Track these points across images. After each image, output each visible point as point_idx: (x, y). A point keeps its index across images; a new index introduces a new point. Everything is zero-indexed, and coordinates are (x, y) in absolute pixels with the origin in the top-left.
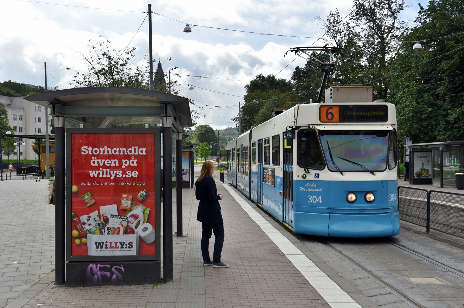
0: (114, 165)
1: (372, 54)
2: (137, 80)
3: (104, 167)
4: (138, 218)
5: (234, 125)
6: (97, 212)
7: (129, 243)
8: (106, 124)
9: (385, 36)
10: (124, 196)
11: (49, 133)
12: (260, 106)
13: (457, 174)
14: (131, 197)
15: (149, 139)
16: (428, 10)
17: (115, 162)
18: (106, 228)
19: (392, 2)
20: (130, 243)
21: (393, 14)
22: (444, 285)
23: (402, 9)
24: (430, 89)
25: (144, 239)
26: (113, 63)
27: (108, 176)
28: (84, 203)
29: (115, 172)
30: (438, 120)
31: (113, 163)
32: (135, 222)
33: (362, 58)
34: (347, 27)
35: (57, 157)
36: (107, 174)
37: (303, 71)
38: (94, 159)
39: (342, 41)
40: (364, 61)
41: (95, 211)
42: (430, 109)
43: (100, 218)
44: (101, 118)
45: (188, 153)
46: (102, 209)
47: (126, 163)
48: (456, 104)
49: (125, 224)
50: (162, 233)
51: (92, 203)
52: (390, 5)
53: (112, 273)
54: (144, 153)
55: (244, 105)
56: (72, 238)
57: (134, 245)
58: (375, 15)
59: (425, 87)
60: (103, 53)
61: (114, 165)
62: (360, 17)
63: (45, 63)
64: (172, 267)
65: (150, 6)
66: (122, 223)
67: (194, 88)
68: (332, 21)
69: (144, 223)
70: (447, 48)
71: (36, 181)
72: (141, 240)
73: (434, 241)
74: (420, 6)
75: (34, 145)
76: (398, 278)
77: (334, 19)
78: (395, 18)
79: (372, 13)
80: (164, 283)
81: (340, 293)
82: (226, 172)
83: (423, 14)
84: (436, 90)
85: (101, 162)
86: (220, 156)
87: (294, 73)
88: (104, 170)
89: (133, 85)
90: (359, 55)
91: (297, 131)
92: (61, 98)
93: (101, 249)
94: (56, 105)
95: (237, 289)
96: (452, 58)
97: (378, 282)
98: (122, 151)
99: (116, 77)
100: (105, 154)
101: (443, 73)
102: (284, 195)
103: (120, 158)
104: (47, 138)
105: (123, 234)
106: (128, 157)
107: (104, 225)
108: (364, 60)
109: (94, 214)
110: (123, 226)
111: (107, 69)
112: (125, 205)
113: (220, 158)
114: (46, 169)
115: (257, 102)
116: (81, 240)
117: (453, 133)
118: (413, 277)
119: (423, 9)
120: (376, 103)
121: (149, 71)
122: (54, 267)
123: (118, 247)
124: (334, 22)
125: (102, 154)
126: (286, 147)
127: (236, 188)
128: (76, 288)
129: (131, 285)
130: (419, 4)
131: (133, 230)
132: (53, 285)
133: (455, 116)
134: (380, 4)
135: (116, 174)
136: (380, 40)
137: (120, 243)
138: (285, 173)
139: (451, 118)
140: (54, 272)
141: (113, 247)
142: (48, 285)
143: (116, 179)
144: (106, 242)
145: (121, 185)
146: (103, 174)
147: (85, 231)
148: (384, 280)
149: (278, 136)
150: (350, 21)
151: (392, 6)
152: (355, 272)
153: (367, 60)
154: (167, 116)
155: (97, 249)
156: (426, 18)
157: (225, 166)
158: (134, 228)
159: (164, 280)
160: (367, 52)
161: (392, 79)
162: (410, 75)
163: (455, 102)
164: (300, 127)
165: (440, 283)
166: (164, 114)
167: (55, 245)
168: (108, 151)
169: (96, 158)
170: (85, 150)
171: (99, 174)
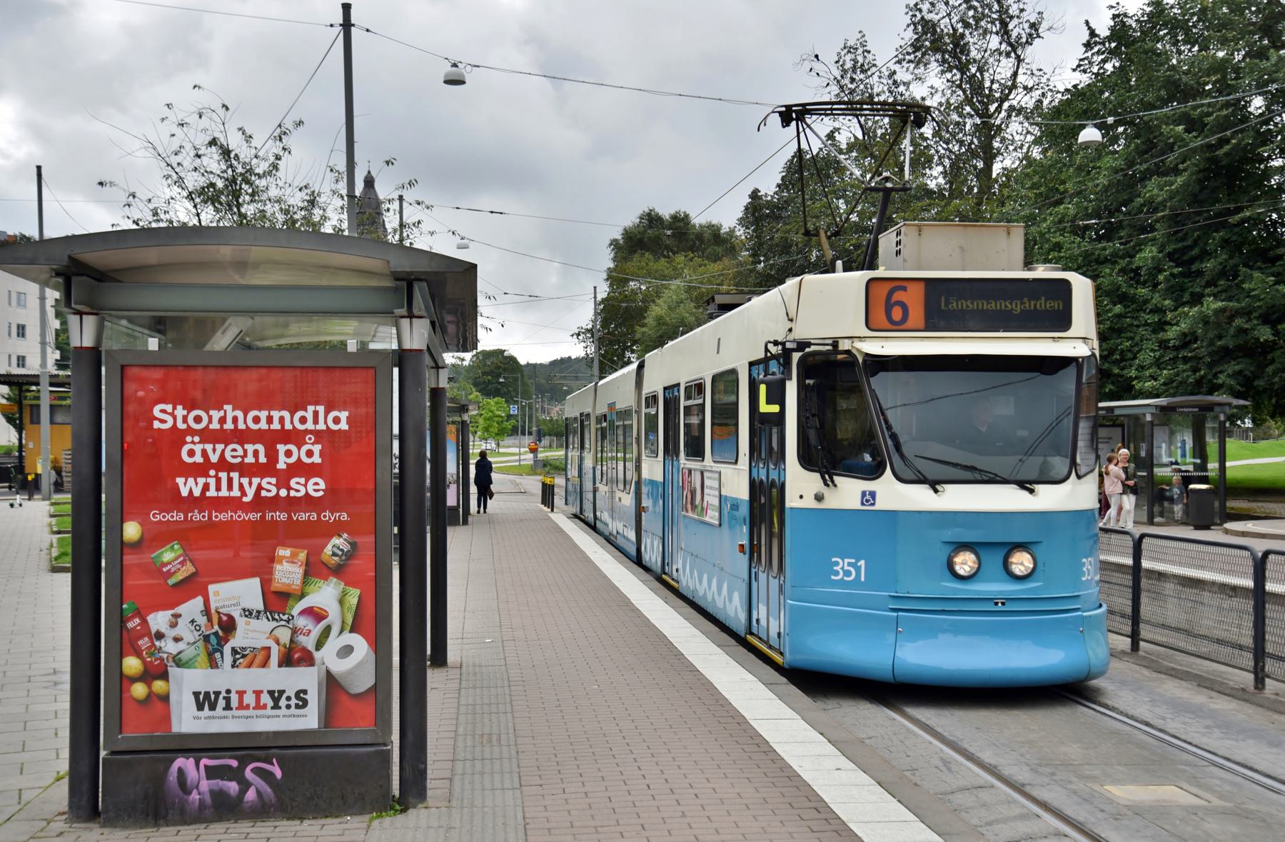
1: (958, 157)
2: (307, 220)
3: (223, 465)
4: (324, 617)
5: (577, 350)
6: (200, 599)
7: (297, 694)
8: (221, 342)
10: (284, 552)
11: (52, 369)
14: (302, 555)
15: (356, 385)
16: (1109, 39)
17: (254, 452)
18: (227, 649)
19: (1011, 18)
20: (301, 694)
21: (1014, 48)
22: (1205, 808)
23: (1039, 36)
24: (1115, 254)
26: (240, 170)
27: (236, 493)
28: (159, 572)
29: (256, 481)
30: (1137, 338)
31: (250, 454)
32: (317, 630)
33: (931, 168)
34: (890, 82)
35: (76, 437)
36: (230, 487)
37: (771, 201)
38: (193, 442)
40: (936, 178)
42: (1118, 309)
43: (210, 620)
44: (207, 324)
46: (216, 593)
47: (288, 454)
48: (1186, 297)
49: (284, 635)
50: (396, 658)
51: (186, 574)
52: (1004, 25)
53: (245, 785)
54: (344, 426)
55: (605, 295)
56: (124, 681)
57: (313, 698)
58: (965, 49)
59: (1104, 249)
60: (210, 139)
62: (924, 54)
63: (39, 168)
64: (425, 763)
65: (347, 8)
66: (276, 632)
67: (471, 244)
68: (849, 65)
70: (1161, 145)
71: (12, 505)
72: (332, 684)
73: (1155, 675)
74: (1089, 28)
75: (4, 402)
77: (855, 61)
79: (956, 45)
82: (559, 481)
83: (1096, 49)
84: (1132, 256)
85: (214, 450)
86: (540, 435)
87: (747, 208)
88: (223, 475)
91: (796, 356)
92: (92, 257)
93: (212, 713)
94: (74, 279)
95: (619, 829)
96: (1176, 171)
98: (276, 420)
99: (249, 210)
100: (225, 427)
102: (753, 551)
103: (271, 439)
104: (45, 382)
105: (280, 666)
106: (295, 437)
107: (222, 641)
108: (935, 173)
109: (192, 608)
110: (278, 642)
112: (284, 580)
114: (39, 471)
115: (643, 288)
116: (149, 686)
118: (1116, 782)
119: (1098, 36)
120: (1042, 272)
122: (64, 766)
124: (854, 69)
125: (218, 427)
126: (764, 408)
127: (593, 527)
129: (302, 819)
130: (1087, 23)
131: (310, 653)
132: (61, 824)
133: (1184, 326)
134: (978, 20)
135: (260, 488)
136: (978, 121)
137: (271, 693)
138: (755, 487)
139: (1172, 333)
140: (66, 780)
141: (248, 707)
142: (44, 823)
143: (260, 502)
144: (228, 691)
145: (273, 521)
146: (218, 489)
147: (162, 659)
148: (1036, 793)
149: (733, 372)
151: (1011, 27)
152: (949, 769)
154: (411, 316)
155: (200, 714)
156: (1104, 61)
158: (311, 647)
159: (399, 802)
162: (1064, 216)
163: (1183, 290)
164: (809, 344)
166: (403, 311)
167: (67, 698)
168: (235, 420)
169: (197, 439)
170: (166, 416)
171: (206, 487)
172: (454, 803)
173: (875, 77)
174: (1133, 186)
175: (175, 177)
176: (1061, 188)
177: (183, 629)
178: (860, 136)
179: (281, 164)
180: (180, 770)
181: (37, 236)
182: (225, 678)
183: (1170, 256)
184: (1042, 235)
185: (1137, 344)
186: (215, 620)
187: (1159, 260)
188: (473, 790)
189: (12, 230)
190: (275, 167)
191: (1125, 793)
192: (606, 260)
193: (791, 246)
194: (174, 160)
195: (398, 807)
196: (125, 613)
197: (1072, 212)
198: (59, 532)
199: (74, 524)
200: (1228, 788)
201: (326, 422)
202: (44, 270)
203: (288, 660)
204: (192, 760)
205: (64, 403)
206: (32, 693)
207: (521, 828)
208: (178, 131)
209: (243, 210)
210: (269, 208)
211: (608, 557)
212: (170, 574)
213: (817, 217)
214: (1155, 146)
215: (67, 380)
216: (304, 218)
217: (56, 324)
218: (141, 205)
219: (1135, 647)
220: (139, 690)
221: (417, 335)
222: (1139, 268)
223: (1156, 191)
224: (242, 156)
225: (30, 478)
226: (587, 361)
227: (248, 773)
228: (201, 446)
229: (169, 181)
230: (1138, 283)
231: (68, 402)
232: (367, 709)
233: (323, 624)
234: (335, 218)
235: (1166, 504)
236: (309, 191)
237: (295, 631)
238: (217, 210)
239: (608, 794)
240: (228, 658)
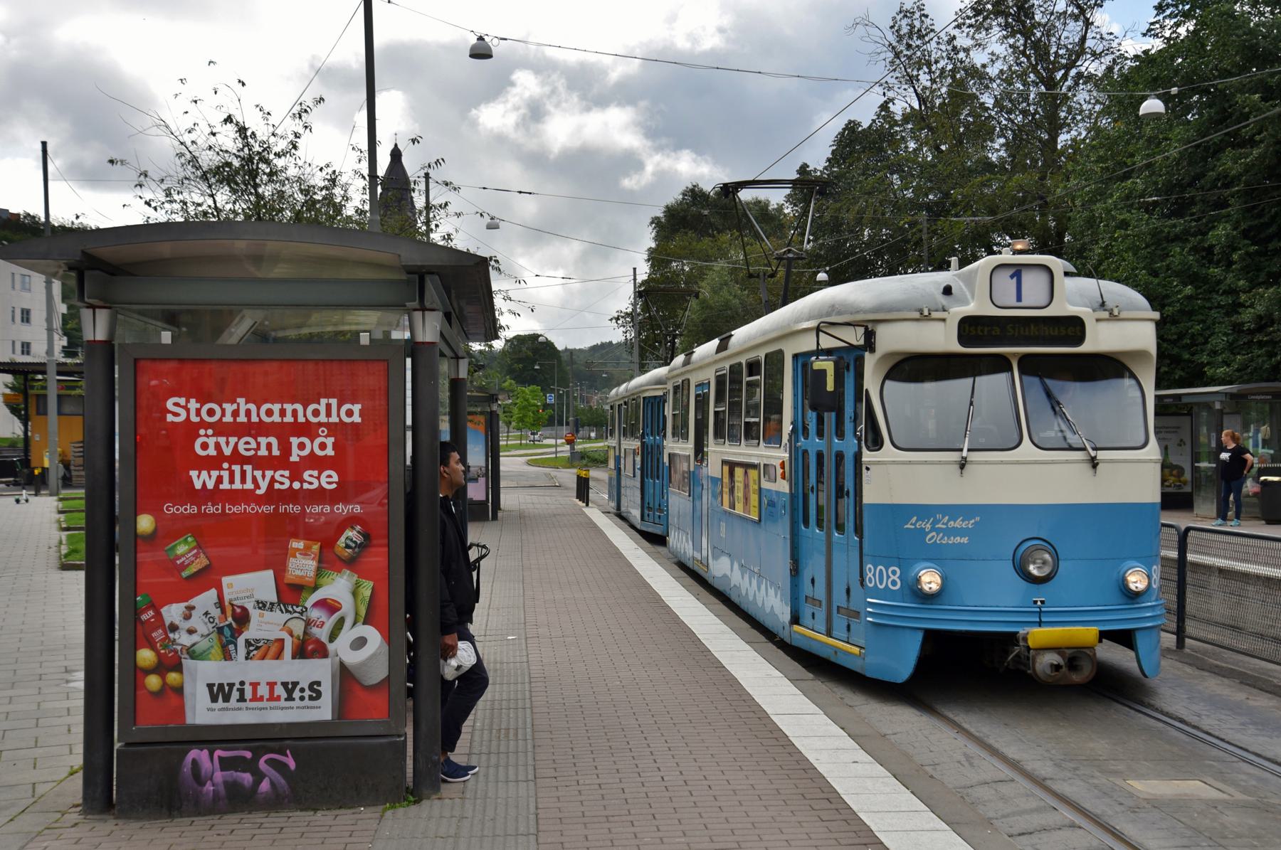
1: (1021, 128)
2: (329, 199)
3: (236, 458)
4: (339, 609)
5: (617, 335)
8: (237, 332)
9: (1059, 75)
10: (297, 544)
11: (59, 356)
17: (267, 445)
18: (241, 641)
20: (314, 687)
24: (1186, 232)
26: (257, 148)
27: (249, 485)
28: (174, 567)
29: (269, 473)
31: (263, 446)
32: (330, 622)
33: (992, 141)
34: (950, 48)
36: (243, 480)
39: (933, 91)
42: (1189, 290)
44: (221, 317)
45: (482, 419)
46: (230, 586)
49: (298, 627)
53: (259, 776)
54: (357, 418)
55: (645, 277)
56: (138, 673)
57: (326, 690)
59: (1174, 226)
60: (225, 116)
62: (985, 19)
63: (44, 144)
66: (289, 624)
67: (501, 224)
68: (905, 30)
69: (355, 624)
71: (18, 501)
72: (345, 675)
73: (1197, 672)
75: (8, 391)
77: (912, 26)
78: (1088, 24)
80: (415, 802)
81: (927, 827)
82: (594, 473)
83: (1168, 12)
84: (1205, 234)
85: (227, 443)
86: (578, 426)
88: (236, 468)
90: (983, 131)
92: (104, 251)
93: (226, 705)
94: (87, 274)
96: (1252, 143)
98: (289, 413)
99: (267, 191)
100: (239, 420)
103: (284, 432)
104: (52, 370)
105: (294, 657)
106: (307, 430)
107: (236, 633)
109: (206, 600)
110: (291, 635)
112: (298, 573)
113: (577, 431)
114: (46, 465)
115: (687, 269)
116: (163, 678)
117: (1252, 360)
118: (1140, 777)
122: (78, 760)
123: (278, 698)
124: (910, 34)
128: (147, 824)
129: (315, 810)
132: (76, 816)
133: (1260, 308)
135: (273, 480)
137: (285, 685)
139: (1246, 316)
140: (80, 774)
141: (261, 699)
142: (59, 815)
143: (273, 495)
144: (242, 683)
146: (232, 481)
147: (175, 651)
148: (1056, 787)
150: (956, 32)
152: (971, 764)
153: (1006, 145)
154: (423, 309)
155: (214, 705)
156: (1177, 25)
157: (591, 455)
158: (324, 639)
160: (1004, 122)
161: (1078, 203)
163: (1259, 270)
165: (1215, 794)
166: (415, 304)
168: (248, 413)
170: (179, 409)
171: (220, 480)
173: (933, 44)
174: (1204, 159)
176: (1129, 161)
177: (197, 621)
178: (917, 107)
179: (301, 143)
181: (43, 219)
182: (240, 670)
183: (1245, 234)
184: (1108, 211)
185: (1209, 328)
186: (229, 612)
188: (487, 782)
189: (15, 208)
190: (295, 147)
191: (1142, 787)
193: (841, 225)
194: (187, 138)
195: (411, 798)
196: (139, 605)
197: (1140, 187)
198: (67, 529)
199: (89, 519)
201: (339, 415)
203: (302, 651)
205: (73, 393)
206: (43, 706)
207: (532, 817)
209: (260, 190)
210: (286, 188)
211: (641, 552)
212: (183, 567)
213: (869, 193)
214: (1231, 115)
215: (76, 369)
216: (325, 198)
217: (63, 308)
218: (153, 185)
219: (1180, 643)
221: (429, 329)
222: (1212, 247)
224: (260, 137)
225: (36, 472)
226: (627, 345)
227: (262, 765)
229: (183, 160)
230: (1210, 262)
231: (78, 391)
234: (356, 199)
236: (330, 170)
237: (308, 623)
238: (234, 191)
239: (622, 785)
240: (242, 650)
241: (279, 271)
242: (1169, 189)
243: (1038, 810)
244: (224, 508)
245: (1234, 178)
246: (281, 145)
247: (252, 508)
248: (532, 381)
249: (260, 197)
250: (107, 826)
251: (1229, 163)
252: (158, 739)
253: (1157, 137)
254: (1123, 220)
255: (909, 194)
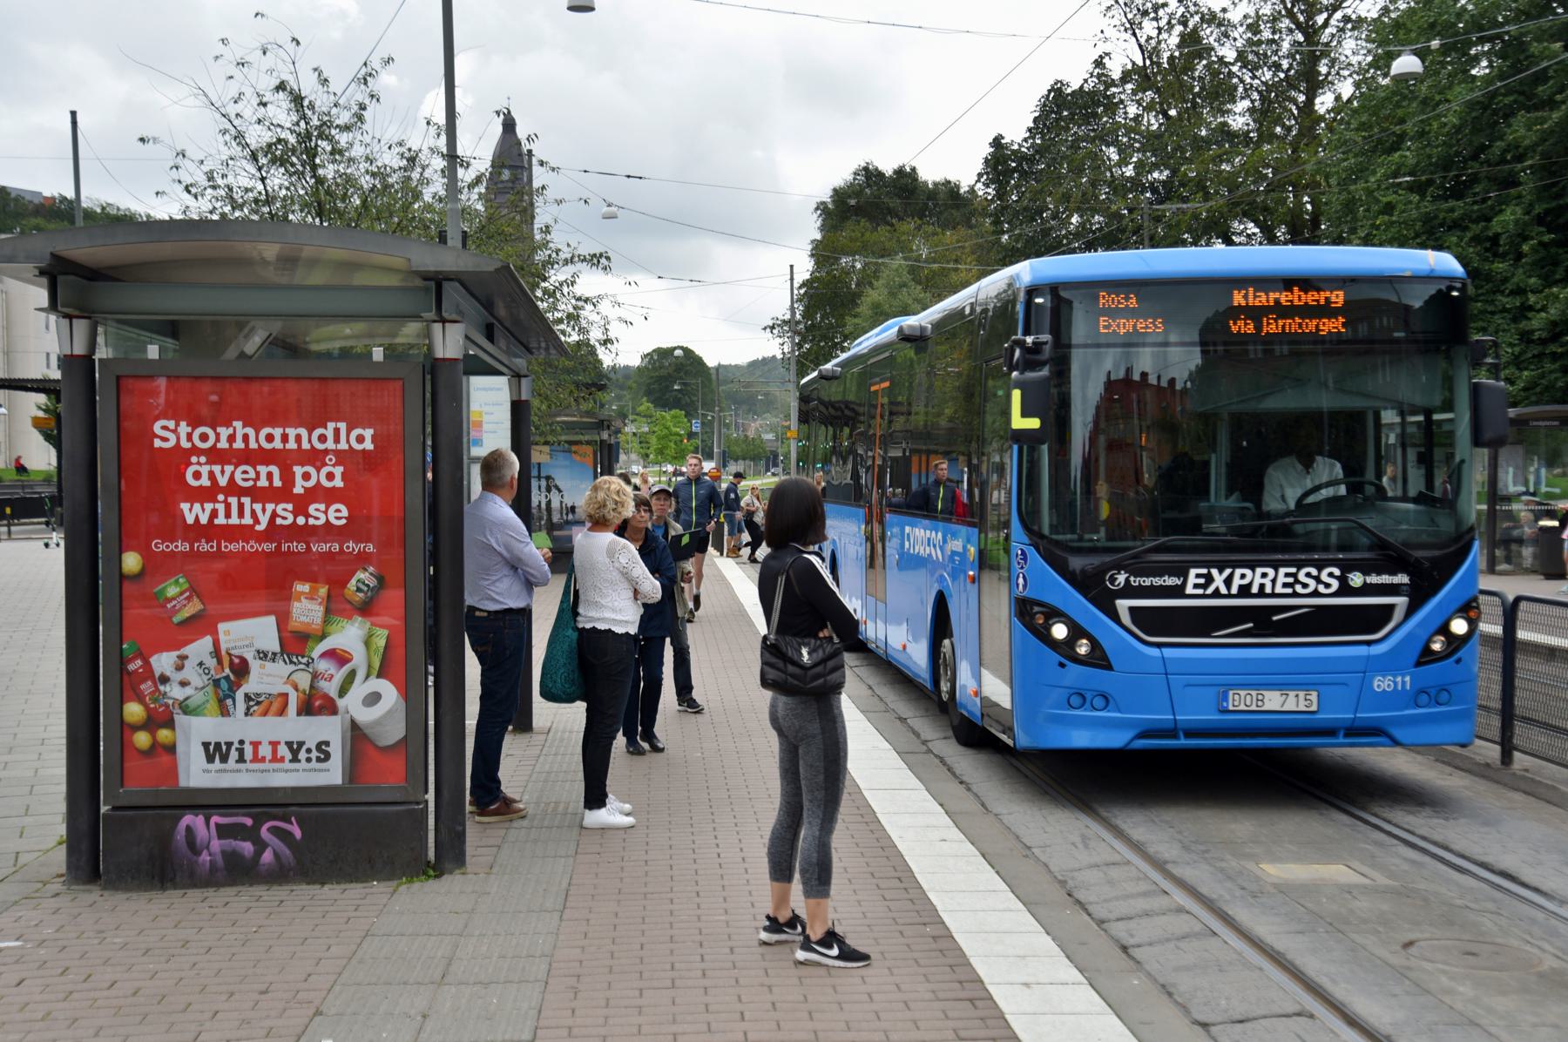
0: (266, 484)
3: (233, 489)
6: (208, 639)
7: (319, 746)
9: (1320, 19)
10: (302, 587)
12: (867, 279)
13: (1542, 523)
14: (323, 591)
17: (268, 475)
18: (240, 695)
20: (322, 747)
22: (1365, 887)
25: (367, 731)
26: (315, 122)
27: (248, 520)
29: (270, 507)
32: (340, 675)
37: (1018, 151)
38: (199, 463)
41: (202, 635)
43: (220, 662)
46: (227, 633)
49: (304, 680)
53: (261, 846)
54: (368, 445)
55: (807, 276)
56: (124, 729)
57: (336, 750)
59: (1452, 210)
60: (277, 82)
61: (266, 484)
63: (73, 114)
66: (294, 677)
67: (620, 213)
69: (367, 677)
71: (47, 545)
72: (357, 734)
75: (41, 414)
76: (1224, 865)
80: (436, 877)
84: (1489, 220)
85: (223, 472)
87: (987, 161)
88: (233, 501)
89: (389, 206)
90: (1221, 91)
93: (223, 766)
94: (60, 279)
97: (1155, 876)
98: (292, 439)
99: (328, 171)
100: (235, 446)
101: (1520, 158)
103: (283, 460)
105: (299, 714)
106: (315, 458)
107: (234, 686)
109: (200, 648)
110: (296, 688)
111: (292, 139)
112: (303, 619)
113: (725, 466)
115: (858, 266)
117: (1542, 376)
121: (445, 150)
123: (282, 759)
125: (227, 446)
128: (134, 895)
129: (323, 884)
131: (331, 701)
133: (1554, 312)
135: (274, 515)
136: (1300, 38)
137: (289, 744)
139: (1537, 322)
144: (242, 742)
145: (289, 553)
146: (228, 516)
147: (167, 706)
152: (1086, 846)
153: (1252, 110)
155: (210, 766)
158: (333, 694)
161: (1333, 181)
162: (1400, 166)
163: (1556, 263)
165: (1355, 879)
166: (432, 315)
168: (246, 438)
169: (203, 459)
170: (168, 434)
171: (214, 514)
172: (495, 870)
175: (233, 132)
180: (189, 829)
182: (238, 727)
183: (1540, 220)
184: (1369, 192)
187: (1525, 224)
190: (360, 118)
191: (1274, 871)
192: (812, 229)
194: (232, 110)
200: (1406, 867)
202: (30, 268)
204: (201, 818)
206: (41, 772)
208: (235, 71)
220: (142, 739)
222: (1497, 236)
223: (1522, 131)
224: (318, 104)
228: (207, 468)
229: (227, 137)
230: (1496, 255)
232: (398, 764)
233: (347, 668)
235: (1514, 547)
237: (315, 676)
241: (318, 278)
242: (1446, 165)
243: (1145, 894)
244: (219, 545)
245: (1527, 148)
246: (344, 118)
247: (253, 546)
248: (676, 404)
249: (320, 181)
250: (93, 895)
251: (1520, 129)
252: (148, 802)
253: (1432, 99)
254: (1389, 204)
255: (1129, 171)
